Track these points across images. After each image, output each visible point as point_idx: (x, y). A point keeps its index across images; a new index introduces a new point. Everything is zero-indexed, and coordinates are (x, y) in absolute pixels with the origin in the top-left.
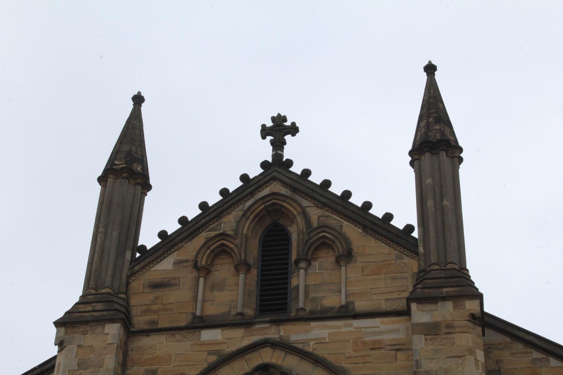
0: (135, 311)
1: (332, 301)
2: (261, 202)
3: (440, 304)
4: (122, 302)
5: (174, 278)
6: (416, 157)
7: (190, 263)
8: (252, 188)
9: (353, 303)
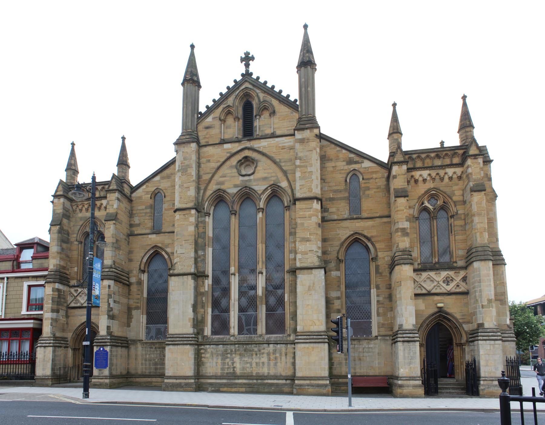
1: (269, 131)
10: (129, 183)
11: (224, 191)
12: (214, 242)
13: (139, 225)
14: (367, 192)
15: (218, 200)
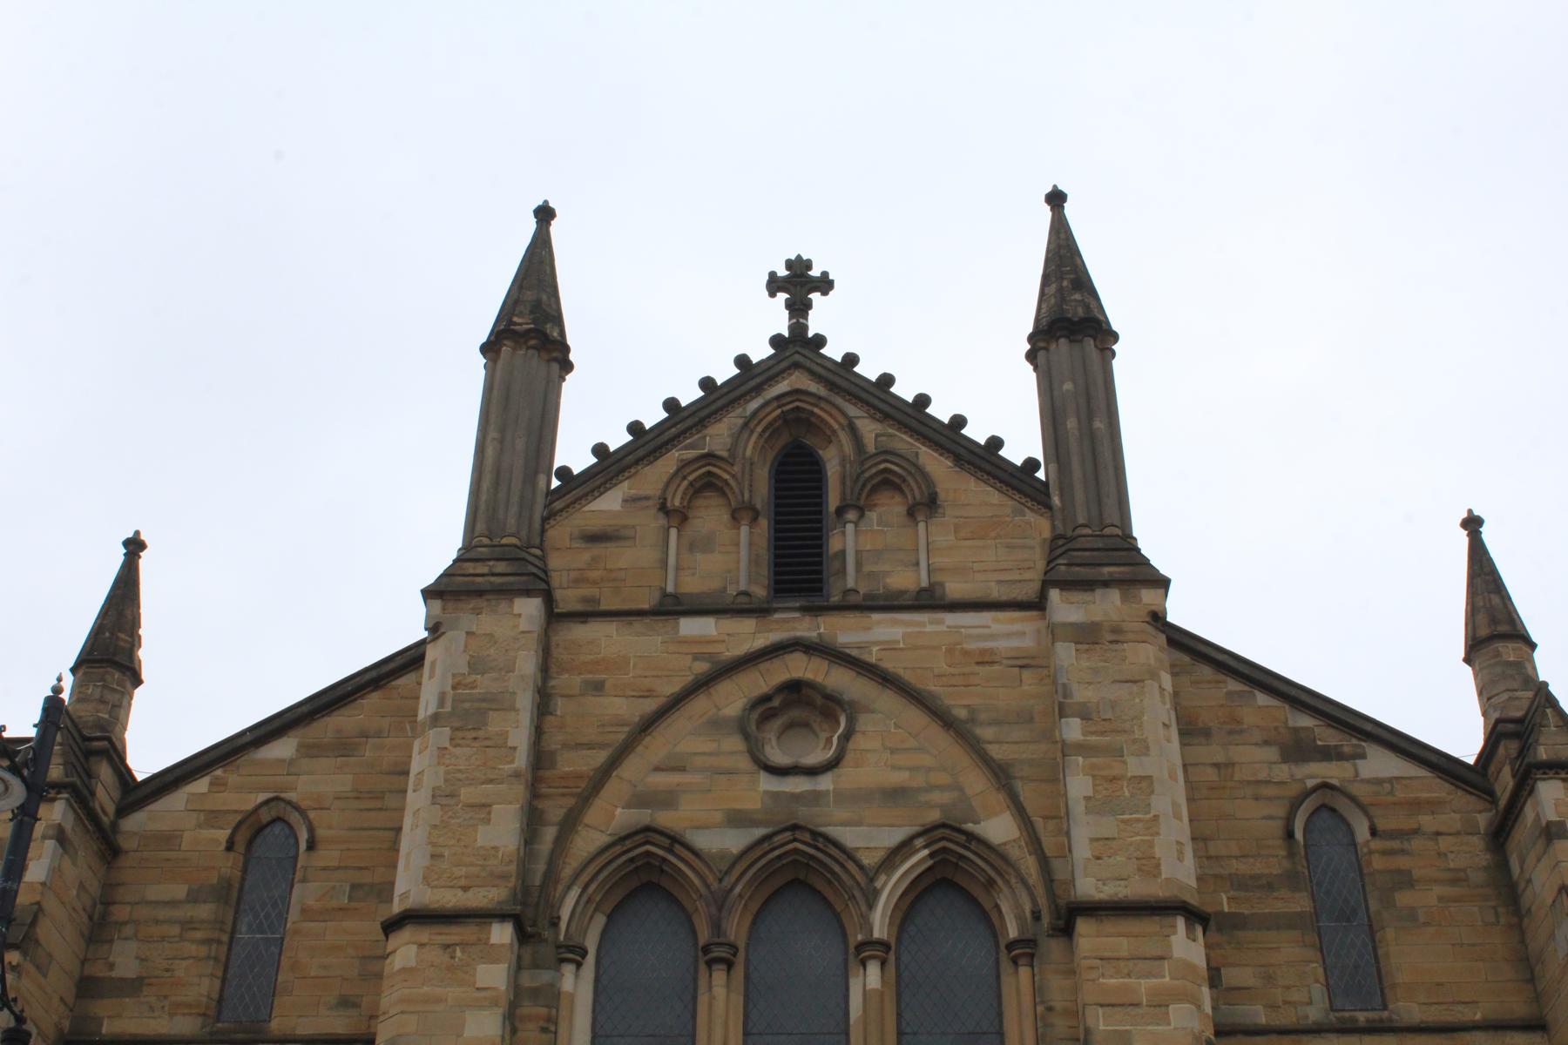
1: (902, 580)
10: (122, 759)
11: (675, 841)
13: (133, 987)
14: (1404, 898)
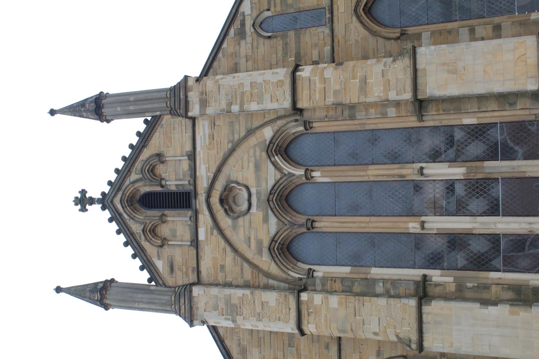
0: (186, 282)
1: (185, 165)
2: (125, 209)
3: (189, 99)
4: (180, 289)
5: (168, 259)
6: (104, 118)
7: (160, 251)
8: (117, 215)
9: (187, 152)
12: (361, 264)
15: (287, 253)
